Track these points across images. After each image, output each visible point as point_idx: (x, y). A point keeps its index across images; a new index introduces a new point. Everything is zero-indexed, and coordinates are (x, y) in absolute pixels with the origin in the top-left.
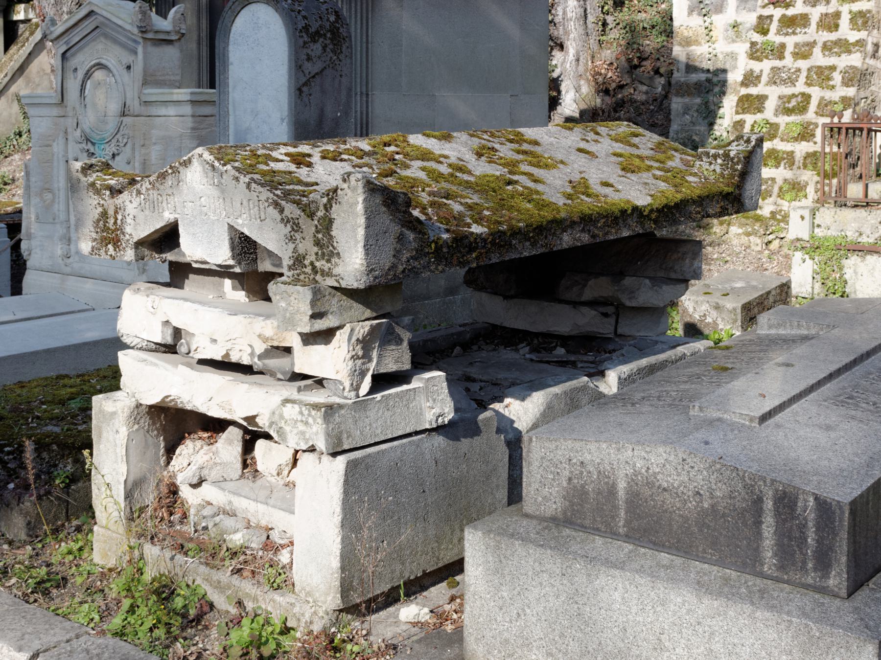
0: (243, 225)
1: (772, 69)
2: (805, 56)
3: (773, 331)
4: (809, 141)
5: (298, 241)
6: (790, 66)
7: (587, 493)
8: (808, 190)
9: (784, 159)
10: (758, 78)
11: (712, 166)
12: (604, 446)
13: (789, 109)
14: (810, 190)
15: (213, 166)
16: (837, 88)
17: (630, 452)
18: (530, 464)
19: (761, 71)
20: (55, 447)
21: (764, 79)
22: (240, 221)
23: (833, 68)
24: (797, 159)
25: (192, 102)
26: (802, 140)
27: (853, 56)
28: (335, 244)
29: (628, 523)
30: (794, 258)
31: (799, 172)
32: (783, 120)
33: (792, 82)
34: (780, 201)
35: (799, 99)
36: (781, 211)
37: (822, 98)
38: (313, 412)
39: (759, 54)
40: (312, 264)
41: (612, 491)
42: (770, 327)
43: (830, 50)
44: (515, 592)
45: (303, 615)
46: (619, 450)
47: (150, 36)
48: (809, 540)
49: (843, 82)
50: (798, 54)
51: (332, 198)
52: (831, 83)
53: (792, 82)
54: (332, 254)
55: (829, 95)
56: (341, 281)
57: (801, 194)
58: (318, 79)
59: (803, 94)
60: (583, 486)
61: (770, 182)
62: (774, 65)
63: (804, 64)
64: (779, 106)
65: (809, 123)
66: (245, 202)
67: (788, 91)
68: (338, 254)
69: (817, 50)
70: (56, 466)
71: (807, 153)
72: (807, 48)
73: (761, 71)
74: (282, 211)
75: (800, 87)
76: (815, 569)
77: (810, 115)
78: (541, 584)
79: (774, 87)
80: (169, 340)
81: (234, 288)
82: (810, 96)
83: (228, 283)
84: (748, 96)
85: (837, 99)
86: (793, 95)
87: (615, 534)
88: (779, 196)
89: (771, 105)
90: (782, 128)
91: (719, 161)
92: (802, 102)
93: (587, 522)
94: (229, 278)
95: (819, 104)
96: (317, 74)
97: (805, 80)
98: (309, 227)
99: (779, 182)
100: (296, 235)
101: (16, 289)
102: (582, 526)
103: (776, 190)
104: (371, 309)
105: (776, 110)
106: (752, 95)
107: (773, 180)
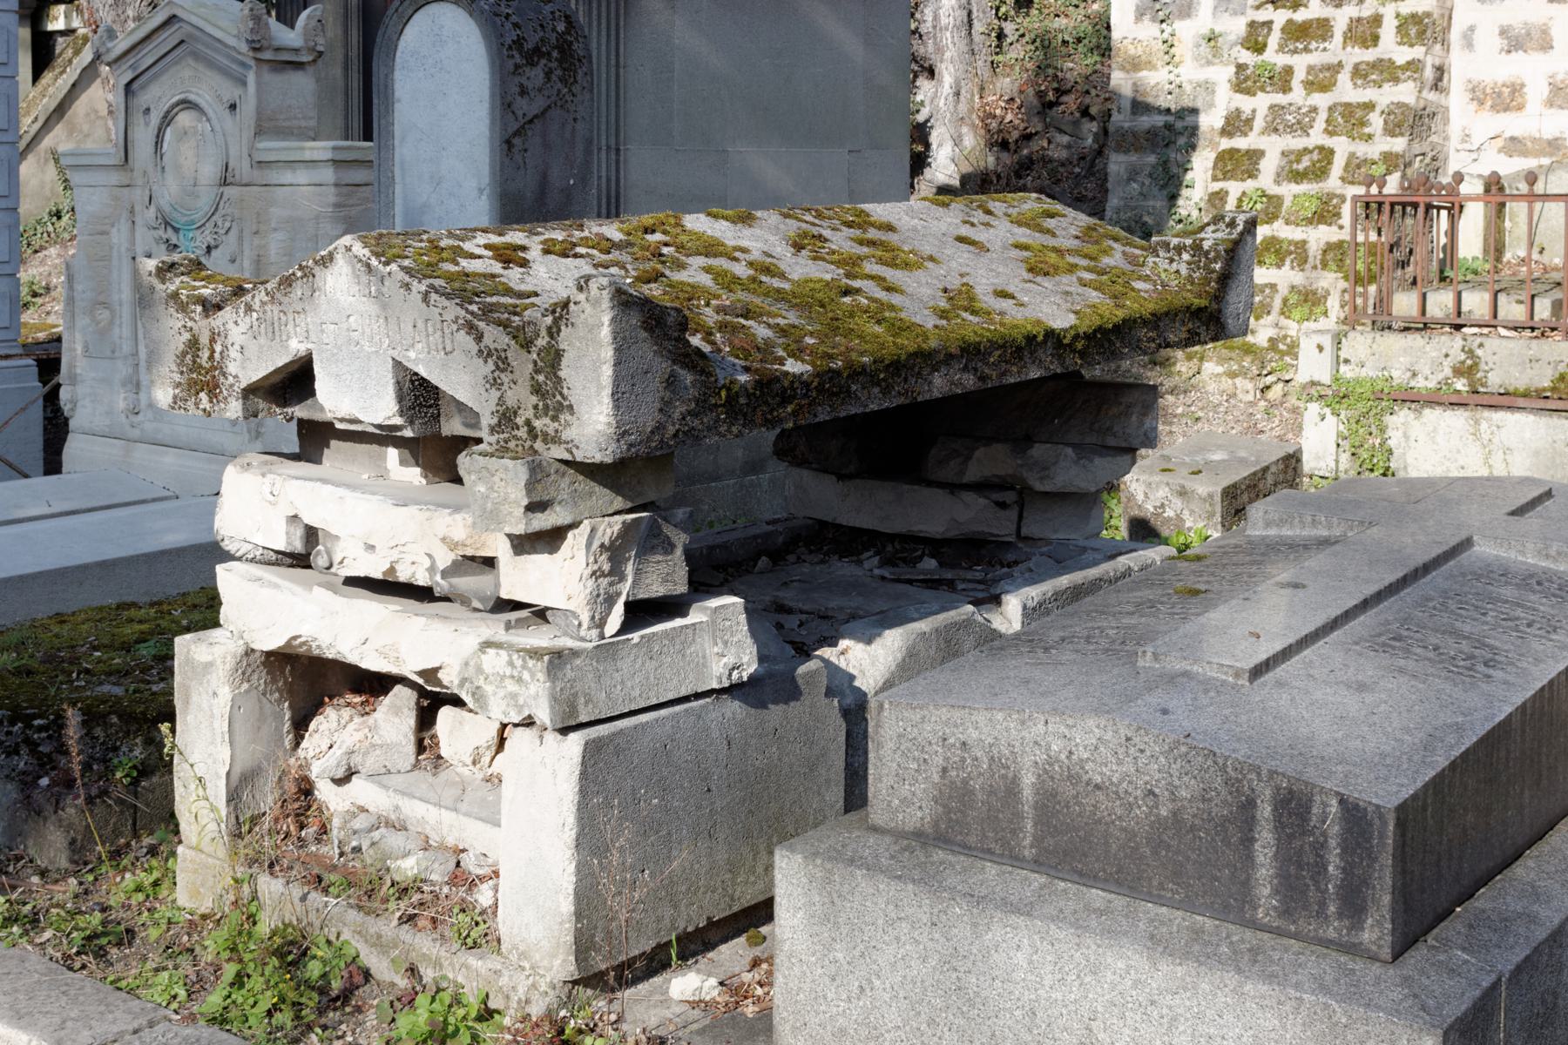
1: (1271, 107)
2: (1325, 87)
3: (1272, 532)
7: (972, 792)
8: (1329, 303)
10: (1249, 122)
12: (1000, 716)
13: (1298, 173)
14: (1333, 303)
15: (368, 266)
16: (1376, 139)
17: (1041, 727)
18: (880, 745)
19: (1254, 111)
20: (114, 719)
21: (1259, 123)
22: (412, 354)
23: (1369, 106)
24: (1311, 254)
25: (336, 163)
26: (1319, 222)
27: (1402, 87)
28: (565, 391)
29: (1038, 841)
31: (1314, 274)
32: (1288, 190)
33: (1303, 128)
34: (1284, 322)
35: (1315, 156)
36: (1285, 337)
37: (1352, 155)
38: (531, 663)
39: (1249, 83)
40: (528, 423)
41: (1012, 789)
42: (1268, 525)
43: (1365, 76)
44: (857, 953)
46: (1023, 723)
47: (267, 55)
48: (1331, 868)
50: (1312, 83)
51: (561, 317)
52: (1367, 130)
54: (560, 408)
58: (538, 124)
59: (1321, 149)
60: (965, 782)
61: (1267, 291)
63: (1322, 100)
65: (1331, 196)
66: (420, 324)
67: (1297, 143)
68: (571, 407)
69: (1344, 78)
70: (116, 749)
73: (1254, 111)
74: (479, 338)
75: (1317, 137)
76: (1340, 915)
77: (1333, 182)
78: (898, 939)
79: (1274, 137)
80: (298, 546)
82: (1332, 152)
83: (392, 453)
84: (1232, 152)
85: (1376, 157)
86: (1305, 149)
87: (1017, 858)
89: (1269, 165)
90: (1287, 203)
91: (1186, 256)
92: (1319, 161)
93: (972, 840)
95: (1347, 165)
96: (536, 116)
97: (1324, 125)
98: (523, 364)
99: (1283, 290)
101: (53, 466)
102: (965, 846)
103: (1277, 303)
104: (623, 496)
105: (1278, 175)
106: (1238, 151)
107: (1273, 286)
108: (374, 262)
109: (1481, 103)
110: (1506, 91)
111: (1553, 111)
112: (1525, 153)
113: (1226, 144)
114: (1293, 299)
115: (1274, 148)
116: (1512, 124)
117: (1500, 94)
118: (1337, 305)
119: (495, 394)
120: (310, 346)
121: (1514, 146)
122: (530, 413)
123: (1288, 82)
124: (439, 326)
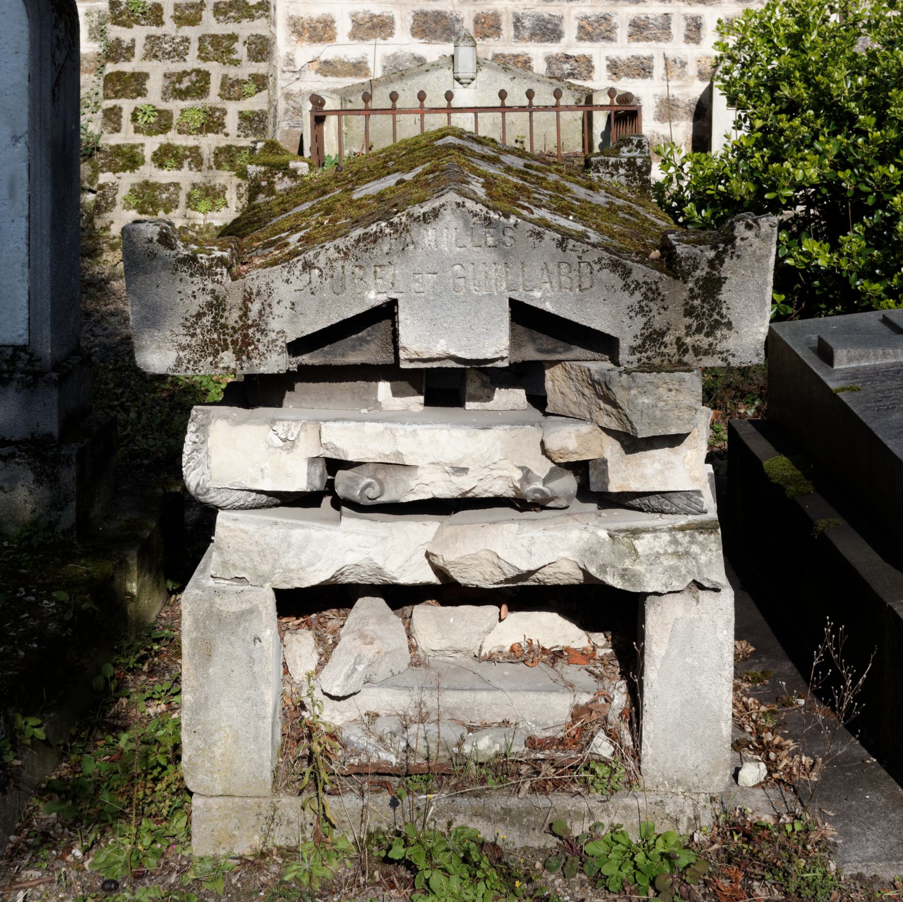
0: (543, 299)
1: (148, 37)
3: (854, 365)
4: (217, 133)
5: (654, 313)
6: (174, 34)
8: (227, 196)
9: (187, 157)
10: (130, 49)
11: (615, 178)
13: (181, 91)
15: (487, 219)
16: (244, 63)
19: (133, 41)
21: (139, 51)
22: (537, 294)
23: (233, 38)
26: (208, 131)
27: (257, 22)
28: (724, 311)
30: (724, 285)
31: (211, 173)
32: (175, 106)
33: (182, 56)
34: (190, 213)
35: (194, 77)
36: (194, 226)
37: (225, 77)
38: (700, 538)
39: (124, 17)
40: (679, 342)
42: (850, 360)
43: (225, 14)
45: (682, 812)
49: (249, 56)
51: (725, 251)
52: (234, 57)
53: (182, 56)
54: (717, 325)
55: (233, 72)
56: (730, 359)
57: (219, 202)
59: (198, 72)
61: (172, 189)
62: (151, 33)
63: (192, 33)
64: (167, 88)
65: (214, 110)
66: (551, 266)
67: (177, 67)
68: (729, 325)
69: (207, 14)
71: (217, 148)
72: (193, 11)
73: (133, 41)
74: (626, 273)
75: (192, 62)
77: (213, 98)
79: (155, 62)
81: (395, 394)
82: (207, 74)
83: (384, 388)
84: (119, 75)
85: (246, 78)
88: (188, 206)
89: (155, 85)
91: (622, 171)
92: (197, 81)
94: (387, 379)
95: (223, 85)
97: (197, 53)
98: (678, 293)
99: (186, 188)
100: (651, 304)
103: (183, 199)
105: (164, 93)
106: (124, 73)
107: (176, 185)
108: (494, 216)
109: (300, 34)
110: (320, 26)
111: (355, 42)
112: (336, 73)
113: (110, 68)
114: (197, 194)
115: (157, 73)
116: (327, 52)
117: (315, 29)
118: (235, 197)
119: (640, 321)
120: (394, 296)
121: (328, 68)
122: (682, 332)
123: (161, 16)
124: (576, 267)
